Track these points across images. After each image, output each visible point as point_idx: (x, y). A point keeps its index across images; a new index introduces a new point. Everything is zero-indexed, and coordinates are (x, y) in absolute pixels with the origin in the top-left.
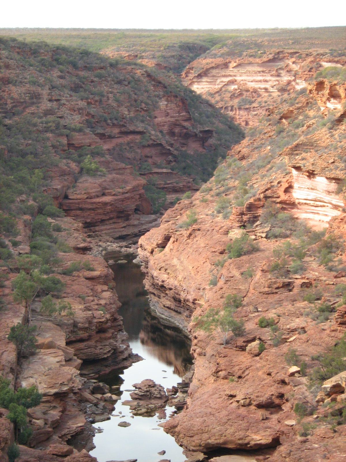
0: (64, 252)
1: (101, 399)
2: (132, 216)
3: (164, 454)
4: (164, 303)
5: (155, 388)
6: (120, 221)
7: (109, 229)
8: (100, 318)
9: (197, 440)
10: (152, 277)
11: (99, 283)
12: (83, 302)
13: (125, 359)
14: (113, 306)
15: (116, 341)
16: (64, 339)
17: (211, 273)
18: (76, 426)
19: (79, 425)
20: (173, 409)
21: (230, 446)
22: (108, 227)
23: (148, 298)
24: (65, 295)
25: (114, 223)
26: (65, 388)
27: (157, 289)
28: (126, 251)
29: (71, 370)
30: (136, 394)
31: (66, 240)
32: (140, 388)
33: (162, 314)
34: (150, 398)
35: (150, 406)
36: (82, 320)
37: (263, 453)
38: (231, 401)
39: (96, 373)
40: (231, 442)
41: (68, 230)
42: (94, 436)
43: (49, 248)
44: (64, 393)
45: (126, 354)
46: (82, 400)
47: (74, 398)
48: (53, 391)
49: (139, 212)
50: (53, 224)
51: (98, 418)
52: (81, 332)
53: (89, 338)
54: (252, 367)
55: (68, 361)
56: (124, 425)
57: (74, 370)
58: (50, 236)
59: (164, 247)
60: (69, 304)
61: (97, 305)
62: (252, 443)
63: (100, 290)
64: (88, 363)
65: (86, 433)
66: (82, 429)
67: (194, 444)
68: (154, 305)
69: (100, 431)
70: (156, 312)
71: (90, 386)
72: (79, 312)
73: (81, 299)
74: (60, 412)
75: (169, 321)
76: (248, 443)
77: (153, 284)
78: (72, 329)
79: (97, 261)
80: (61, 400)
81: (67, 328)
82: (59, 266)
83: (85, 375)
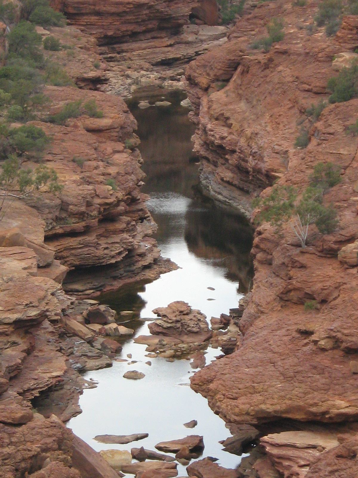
0: (56, 85)
1: (100, 333)
2: (185, 27)
3: (194, 426)
4: (222, 175)
5: (191, 316)
6: (163, 35)
7: (144, 49)
8: (106, 198)
9: (243, 404)
10: (205, 131)
11: (110, 139)
12: (79, 169)
13: (148, 267)
14: (129, 178)
15: (134, 237)
16: (42, 230)
17: (299, 127)
18: (49, 375)
19: (55, 374)
20: (219, 352)
21: (299, 416)
22: (144, 45)
23: (198, 166)
24: (50, 157)
25: (153, 38)
26: (33, 313)
27: (212, 151)
28: (171, 86)
29: (47, 283)
30: (157, 325)
31: (65, 65)
32: (164, 316)
33: (219, 193)
34: (181, 333)
35: (180, 345)
36: (74, 200)
37: (352, 429)
38: (306, 341)
39: (96, 289)
40: (299, 409)
41: (70, 48)
42: (81, 393)
43: (30, 76)
44: (32, 320)
45: (149, 259)
46: (66, 333)
47: (51, 329)
48: (14, 317)
49: (198, 21)
50: (44, 38)
51: (91, 363)
52: (74, 220)
53: (87, 230)
54: (345, 286)
55: (43, 267)
56: (133, 376)
57: (51, 282)
58: (37, 57)
59: (227, 81)
60: (53, 172)
61: (103, 175)
62: (335, 411)
63: (109, 150)
64: (80, 273)
65: (68, 387)
66: (59, 381)
67: (237, 410)
68: (207, 178)
69: (92, 385)
70: (209, 190)
71: (83, 309)
72: (71, 184)
73: (75, 165)
74: (24, 351)
75: (230, 205)
76: (326, 412)
77: (205, 143)
78: (57, 214)
79: (109, 101)
80: (27, 332)
81: (49, 213)
82: (44, 108)
83: (78, 291)
